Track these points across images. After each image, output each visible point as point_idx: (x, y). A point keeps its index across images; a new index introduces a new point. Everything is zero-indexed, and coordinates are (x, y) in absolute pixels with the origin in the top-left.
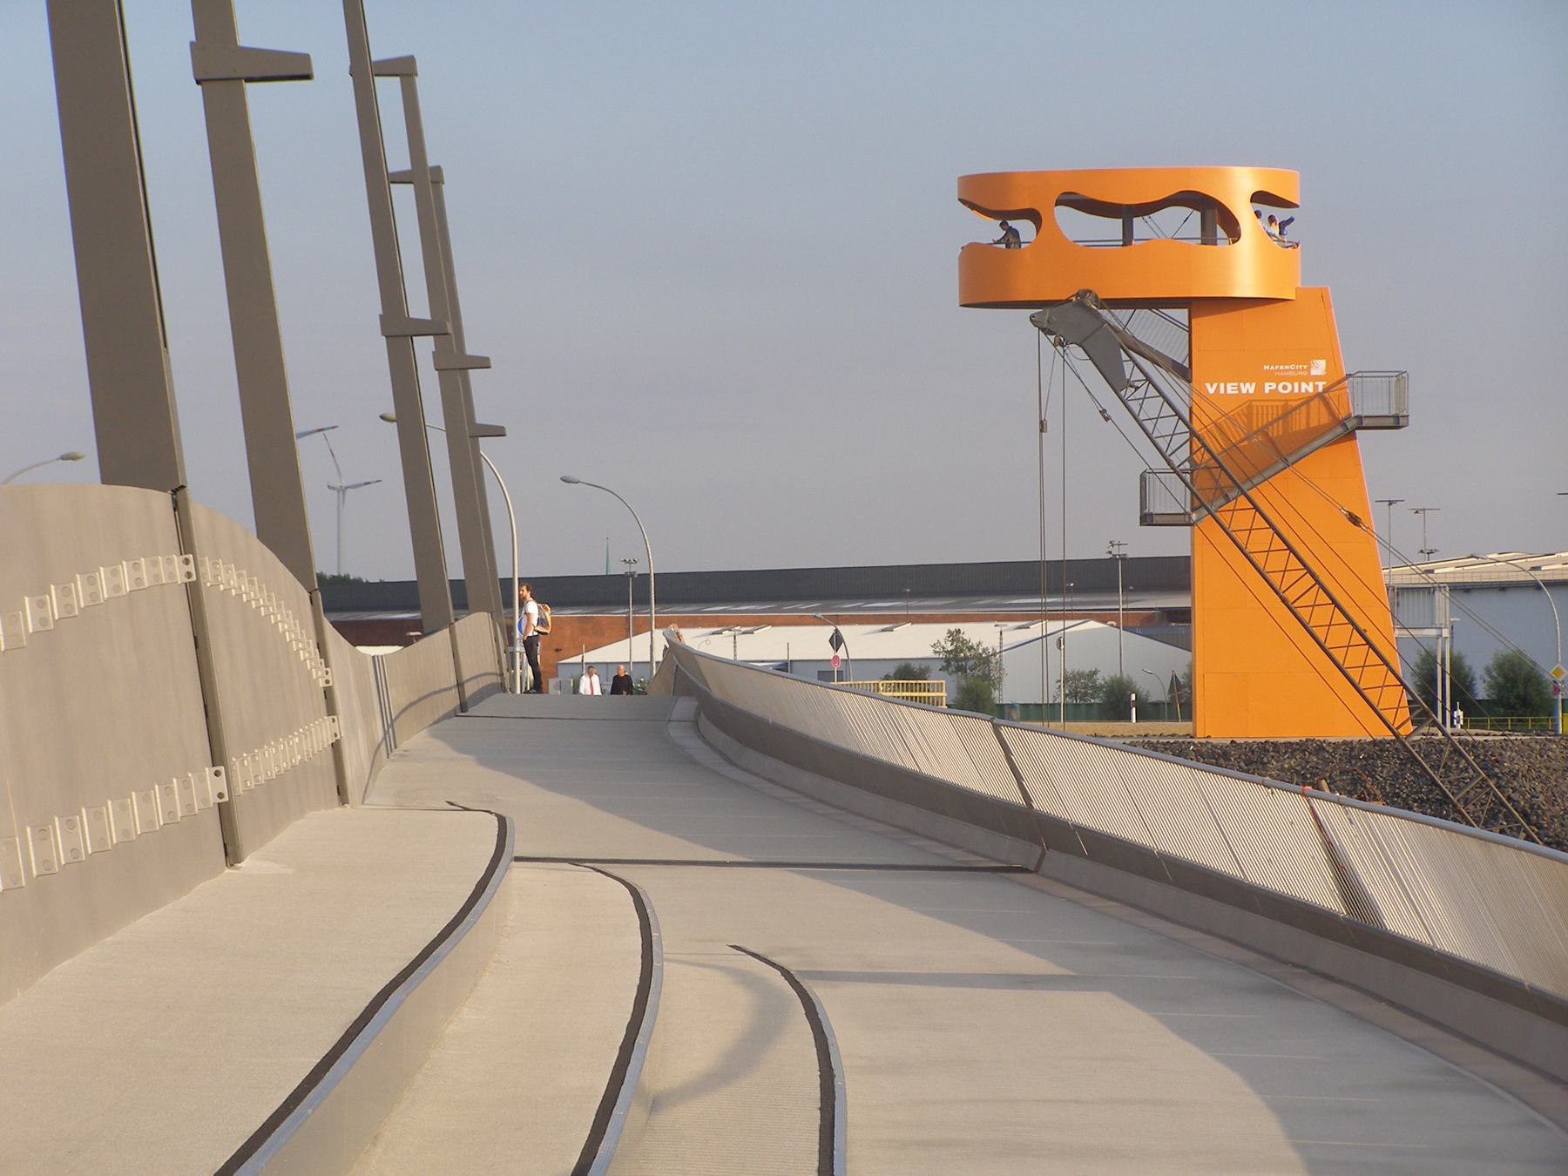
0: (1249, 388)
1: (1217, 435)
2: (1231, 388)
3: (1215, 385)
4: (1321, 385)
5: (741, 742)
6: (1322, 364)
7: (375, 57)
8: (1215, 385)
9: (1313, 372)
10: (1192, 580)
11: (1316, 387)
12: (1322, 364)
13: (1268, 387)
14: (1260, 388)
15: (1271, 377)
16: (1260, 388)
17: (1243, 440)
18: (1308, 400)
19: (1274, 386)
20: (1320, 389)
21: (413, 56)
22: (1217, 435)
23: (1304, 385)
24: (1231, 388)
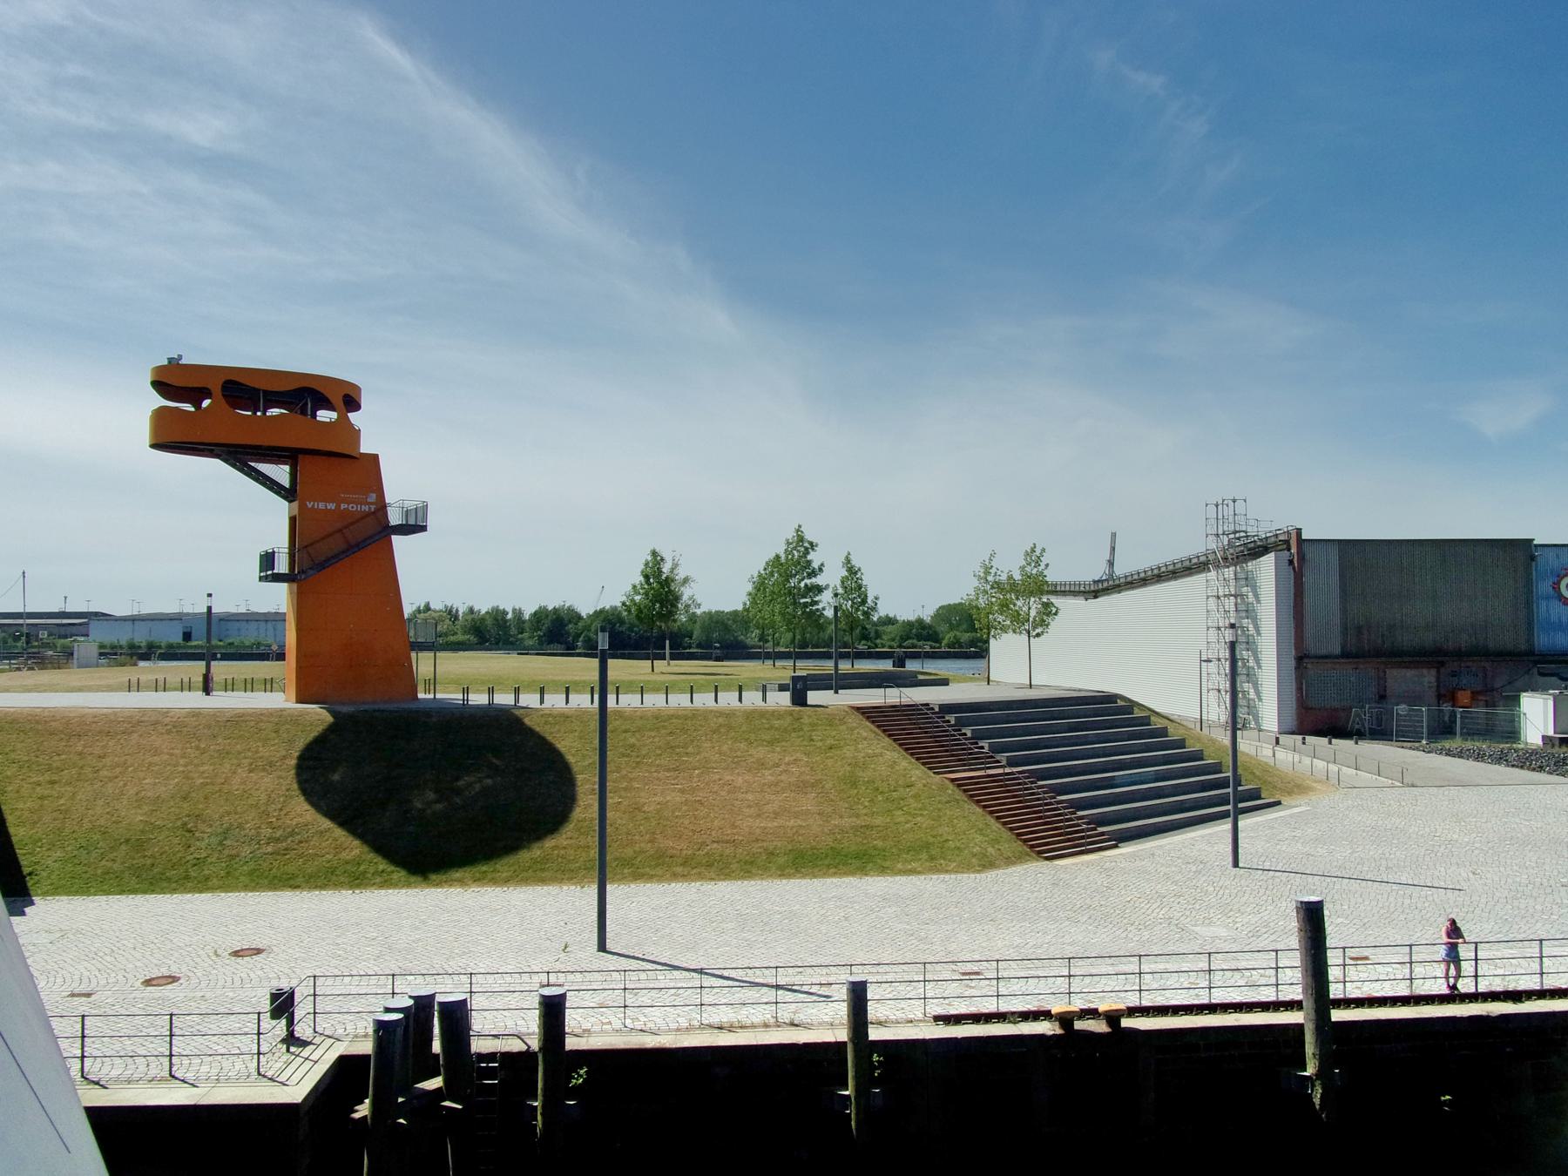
0: (331, 506)
1: (1507, 952)
2: (321, 506)
3: (312, 503)
4: (373, 508)
5: (79, 1099)
6: (374, 495)
7: (598, 660)
8: (312, 503)
9: (369, 500)
10: (1291, 687)
11: (370, 508)
12: (374, 495)
13: (343, 506)
14: (338, 506)
15: (345, 501)
16: (338, 506)
17: (1448, 982)
18: (368, 515)
19: (346, 506)
20: (373, 510)
21: (377, 455)
22: (1507, 952)
23: (363, 506)
24: (321, 506)
